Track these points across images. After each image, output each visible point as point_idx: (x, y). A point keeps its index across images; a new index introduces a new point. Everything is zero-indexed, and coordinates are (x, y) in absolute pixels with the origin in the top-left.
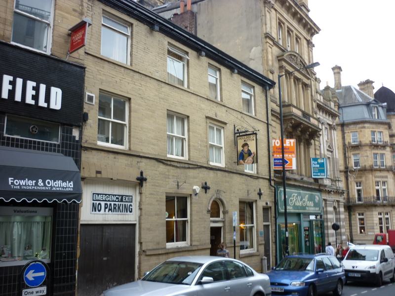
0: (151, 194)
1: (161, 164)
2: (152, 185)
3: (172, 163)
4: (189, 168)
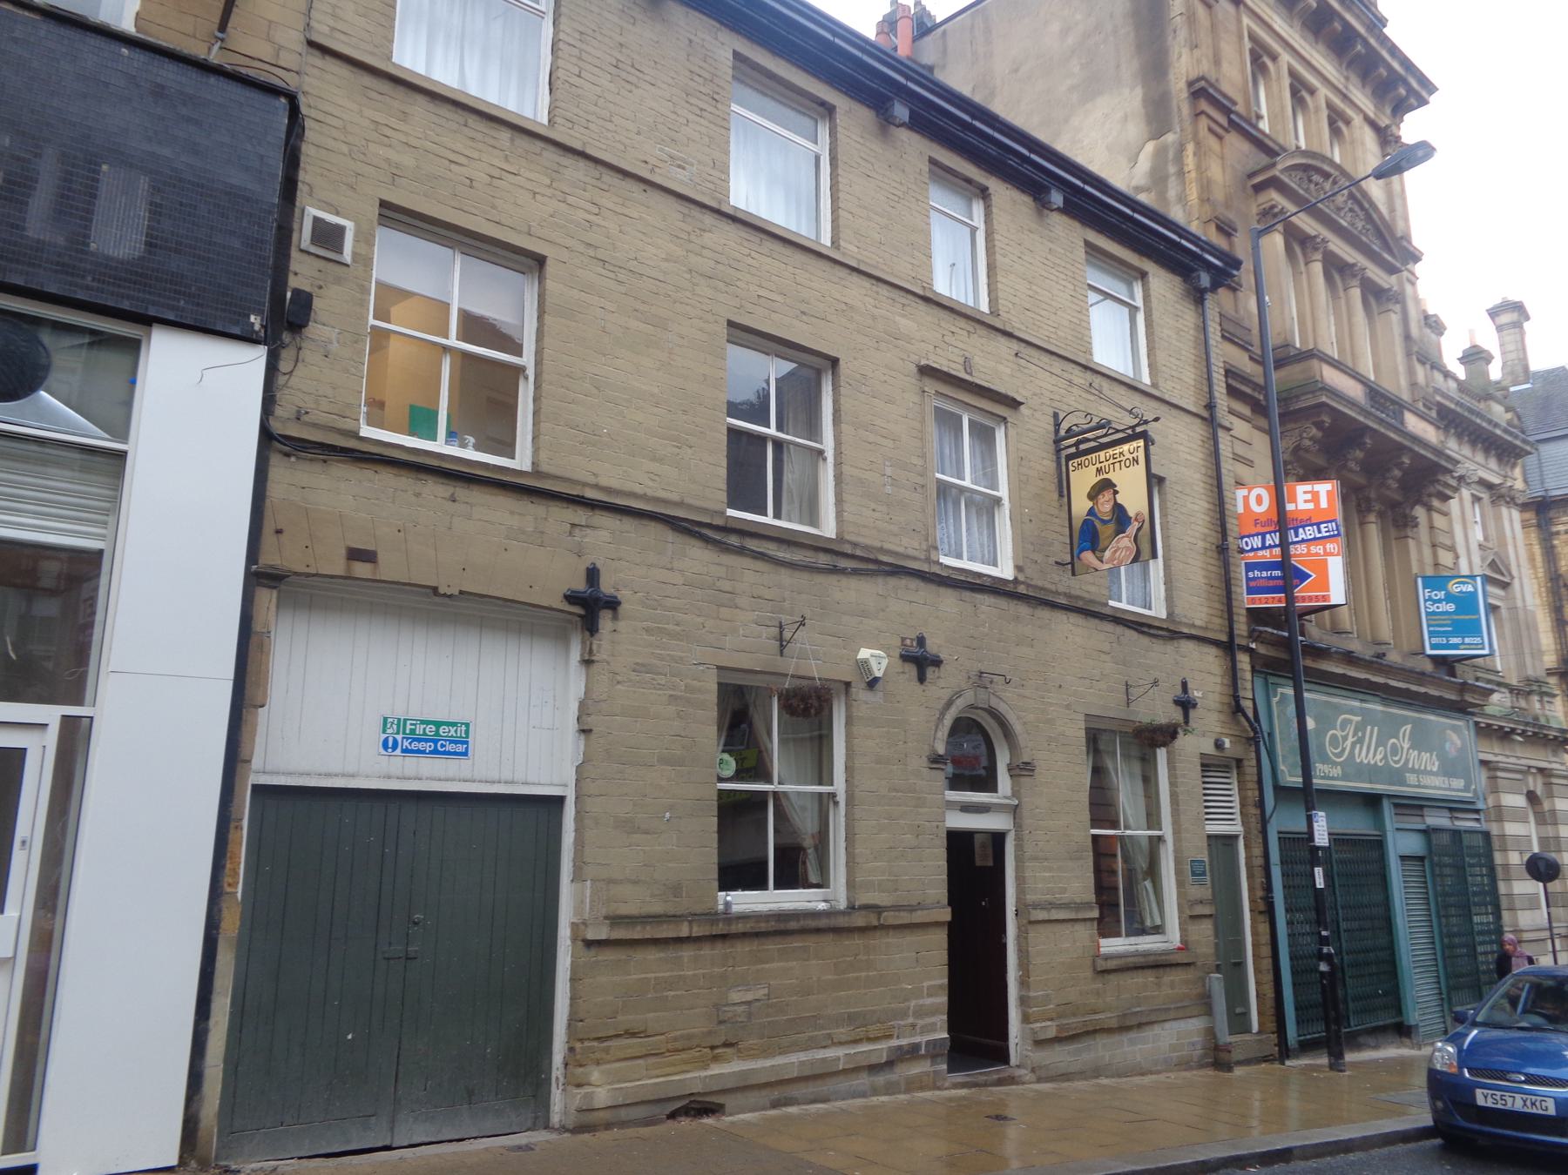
0: (639, 668)
1: (698, 543)
2: (648, 630)
3: (752, 544)
4: (835, 570)
